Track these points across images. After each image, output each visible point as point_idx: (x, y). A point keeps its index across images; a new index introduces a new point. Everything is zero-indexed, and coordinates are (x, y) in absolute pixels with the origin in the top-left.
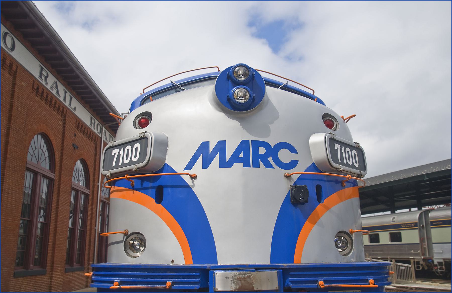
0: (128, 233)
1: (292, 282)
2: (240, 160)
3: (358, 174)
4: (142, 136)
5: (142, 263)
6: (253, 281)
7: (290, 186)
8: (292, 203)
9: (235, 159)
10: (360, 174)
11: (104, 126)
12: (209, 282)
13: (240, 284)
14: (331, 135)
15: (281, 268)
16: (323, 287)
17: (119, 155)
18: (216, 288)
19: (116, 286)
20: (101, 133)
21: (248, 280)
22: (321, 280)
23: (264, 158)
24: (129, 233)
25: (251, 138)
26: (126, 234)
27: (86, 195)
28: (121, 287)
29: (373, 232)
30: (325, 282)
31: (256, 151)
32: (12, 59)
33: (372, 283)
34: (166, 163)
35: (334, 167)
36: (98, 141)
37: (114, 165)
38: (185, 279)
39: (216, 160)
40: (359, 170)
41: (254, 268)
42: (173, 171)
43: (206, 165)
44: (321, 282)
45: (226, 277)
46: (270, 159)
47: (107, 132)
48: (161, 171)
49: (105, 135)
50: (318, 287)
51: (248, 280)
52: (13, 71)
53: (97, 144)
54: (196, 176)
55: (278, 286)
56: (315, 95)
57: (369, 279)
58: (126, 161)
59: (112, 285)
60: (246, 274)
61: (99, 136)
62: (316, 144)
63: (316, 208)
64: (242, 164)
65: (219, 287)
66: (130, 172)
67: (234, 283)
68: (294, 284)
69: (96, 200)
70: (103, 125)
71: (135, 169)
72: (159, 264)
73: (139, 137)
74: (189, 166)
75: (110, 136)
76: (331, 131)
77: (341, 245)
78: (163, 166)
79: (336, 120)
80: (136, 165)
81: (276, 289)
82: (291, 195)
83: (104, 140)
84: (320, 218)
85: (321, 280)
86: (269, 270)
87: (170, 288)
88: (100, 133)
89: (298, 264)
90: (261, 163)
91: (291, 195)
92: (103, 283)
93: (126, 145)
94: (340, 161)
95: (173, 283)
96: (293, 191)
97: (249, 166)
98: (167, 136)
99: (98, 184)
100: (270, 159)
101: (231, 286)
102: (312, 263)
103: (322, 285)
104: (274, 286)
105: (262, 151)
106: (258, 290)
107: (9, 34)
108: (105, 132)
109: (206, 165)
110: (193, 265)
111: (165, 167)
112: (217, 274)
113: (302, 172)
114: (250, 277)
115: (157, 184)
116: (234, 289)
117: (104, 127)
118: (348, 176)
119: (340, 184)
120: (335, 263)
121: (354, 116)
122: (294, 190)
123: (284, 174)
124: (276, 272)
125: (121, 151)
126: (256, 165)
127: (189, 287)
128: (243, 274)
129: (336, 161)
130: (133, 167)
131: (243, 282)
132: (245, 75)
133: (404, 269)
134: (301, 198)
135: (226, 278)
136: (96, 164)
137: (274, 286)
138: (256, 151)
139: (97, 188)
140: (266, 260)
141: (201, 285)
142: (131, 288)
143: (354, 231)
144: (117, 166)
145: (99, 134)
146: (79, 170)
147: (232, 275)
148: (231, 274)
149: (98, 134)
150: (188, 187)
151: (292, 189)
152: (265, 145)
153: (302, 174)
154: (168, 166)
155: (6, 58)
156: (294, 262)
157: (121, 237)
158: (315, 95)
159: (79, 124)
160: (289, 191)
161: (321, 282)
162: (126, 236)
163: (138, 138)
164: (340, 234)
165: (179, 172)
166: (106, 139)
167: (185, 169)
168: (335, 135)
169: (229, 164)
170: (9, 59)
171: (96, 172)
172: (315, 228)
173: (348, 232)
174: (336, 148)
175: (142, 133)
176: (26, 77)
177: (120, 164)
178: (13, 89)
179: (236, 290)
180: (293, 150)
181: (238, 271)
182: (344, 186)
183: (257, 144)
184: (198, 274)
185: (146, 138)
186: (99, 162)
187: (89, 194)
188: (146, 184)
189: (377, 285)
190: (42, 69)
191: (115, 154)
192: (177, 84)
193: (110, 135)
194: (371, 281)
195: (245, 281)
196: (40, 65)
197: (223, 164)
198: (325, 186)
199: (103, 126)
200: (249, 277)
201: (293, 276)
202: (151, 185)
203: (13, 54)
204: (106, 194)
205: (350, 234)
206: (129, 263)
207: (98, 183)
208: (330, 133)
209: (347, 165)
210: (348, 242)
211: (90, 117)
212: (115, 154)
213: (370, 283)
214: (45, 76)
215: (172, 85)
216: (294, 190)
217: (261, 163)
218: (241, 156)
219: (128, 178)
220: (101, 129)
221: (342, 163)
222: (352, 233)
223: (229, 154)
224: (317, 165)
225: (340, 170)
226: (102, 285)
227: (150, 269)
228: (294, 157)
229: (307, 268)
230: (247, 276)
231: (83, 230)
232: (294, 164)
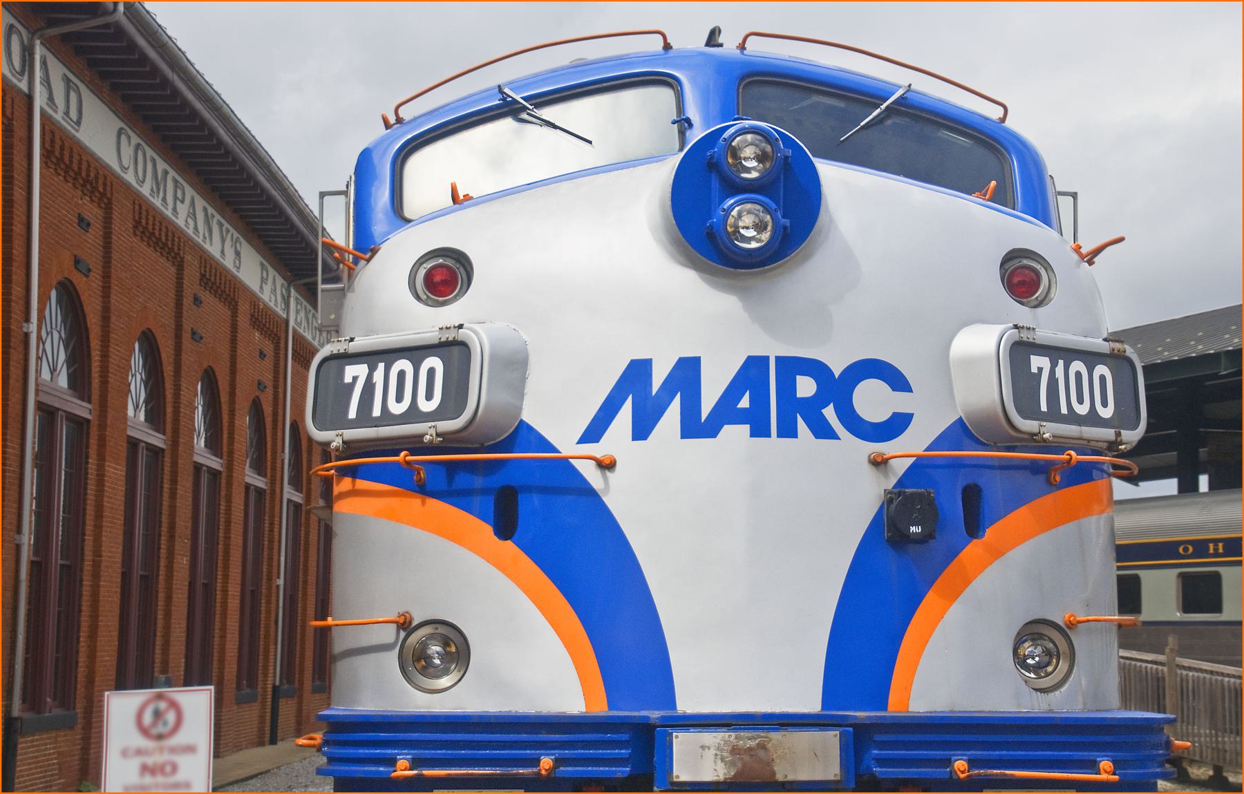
0: (410, 623)
1: (881, 762)
2: (739, 417)
3: (1107, 442)
4: (451, 339)
5: (461, 709)
6: (774, 757)
7: (885, 490)
8: (888, 541)
9: (726, 412)
10: (1116, 439)
11: (38, 34)
12: (655, 759)
13: (739, 765)
14: (1019, 332)
15: (849, 722)
16: (965, 778)
17: (369, 387)
18: (675, 773)
19: (402, 770)
20: (26, 73)
21: (761, 753)
22: (960, 757)
23: (811, 410)
24: (415, 623)
25: (773, 349)
26: (405, 625)
27: (79, 425)
28: (424, 772)
30: (972, 763)
31: (787, 387)
33: (1108, 770)
34: (524, 419)
35: (1023, 430)
36: (16, 113)
37: (352, 414)
38: (590, 750)
39: (673, 414)
40: (1112, 427)
41: (776, 723)
42: (547, 446)
43: (641, 430)
44: (960, 765)
45: (700, 745)
46: (829, 413)
47: (53, 63)
48: (507, 445)
49: (47, 81)
50: (951, 777)
51: (761, 753)
53: (12, 131)
54: (615, 462)
55: (841, 771)
56: (1008, 123)
57: (1100, 759)
58: (397, 409)
59: (391, 769)
60: (755, 739)
61: (20, 91)
62: (970, 362)
63: (960, 555)
64: (745, 429)
65: (682, 772)
66: (415, 445)
67: (722, 761)
68: (884, 767)
69: (19, 407)
70: (38, 30)
71: (431, 435)
72: (510, 711)
73: (440, 339)
74: (593, 433)
75: (68, 81)
76: (1022, 314)
77: (1037, 659)
78: (513, 428)
79: (1048, 267)
80: (433, 424)
81: (836, 779)
82: (887, 517)
83: (42, 110)
84: (970, 582)
85: (960, 757)
86: (817, 729)
87: (549, 774)
88: (22, 73)
89: (901, 712)
90: (801, 424)
91: (885, 517)
92: (362, 765)
93: (394, 355)
94: (1044, 408)
96: (893, 506)
97: (767, 434)
98: (525, 337)
99: (25, 330)
100: (829, 413)
101: (715, 770)
102: (942, 712)
103: (963, 772)
104: (832, 771)
105: (806, 387)
106: (786, 780)
108: (44, 63)
109: (641, 430)
110: (610, 712)
111: (523, 435)
112: (677, 737)
113: (920, 450)
114: (765, 745)
115: (498, 480)
116: (722, 778)
117: (38, 42)
118: (1068, 455)
119: (1042, 478)
120: (1010, 712)
121: (1121, 240)
122: (895, 503)
123: (869, 456)
124: (834, 733)
125: (375, 373)
126: (788, 431)
127: (603, 771)
128: (748, 740)
129: (1030, 410)
130: (428, 431)
131: (747, 758)
132: (762, 158)
133: (676, 713)
134: (913, 529)
135: (703, 747)
136: (12, 230)
137: (832, 771)
138: (787, 387)
139: (21, 349)
140: (810, 702)
141: (632, 767)
142: (450, 774)
143: (1078, 619)
144: (364, 417)
145: (20, 81)
146: (54, 326)
147: (718, 741)
148: (713, 738)
149: (15, 81)
150: (591, 493)
151: (890, 501)
152: (815, 368)
153: (919, 458)
154: (530, 428)
156: (890, 708)
157: (388, 634)
158: (1008, 123)
159: (64, 149)
160: (879, 506)
161: (960, 765)
162: (404, 629)
163: (436, 341)
164: (1034, 630)
165: (565, 452)
166: (51, 98)
167: (581, 441)
168: (1034, 329)
169: (709, 429)
171: (14, 269)
172: (956, 612)
173: (1060, 624)
174: (1034, 370)
175: (450, 328)
177: (377, 412)
178: (107, 225)
179: (729, 778)
180: (898, 382)
181: (734, 729)
182: (1055, 483)
183: (791, 367)
184: (625, 737)
185: (463, 345)
186: (24, 218)
187: (88, 421)
188: (462, 480)
189: (1118, 777)
191: (355, 379)
192: (518, 98)
193: (220, 222)
194: (1105, 764)
195: (752, 756)
197: (693, 427)
198: (994, 487)
199: (33, 34)
200: (762, 746)
201: (883, 745)
202: (479, 482)
204: (55, 370)
205: (1065, 629)
206: (418, 708)
207: (25, 325)
208: (1016, 327)
209: (1073, 418)
210: (1061, 652)
211: (63, 80)
212: (355, 379)
213: (1102, 771)
215: (504, 99)
216: (895, 503)
217: (801, 424)
218: (745, 403)
219: (408, 463)
220: (27, 52)
221: (1054, 415)
222: (1072, 625)
223: (710, 397)
224: (970, 424)
225: (1043, 438)
226: (362, 769)
227: (510, 724)
229: (925, 725)
230: (757, 742)
231: (67, 566)
232: (897, 425)
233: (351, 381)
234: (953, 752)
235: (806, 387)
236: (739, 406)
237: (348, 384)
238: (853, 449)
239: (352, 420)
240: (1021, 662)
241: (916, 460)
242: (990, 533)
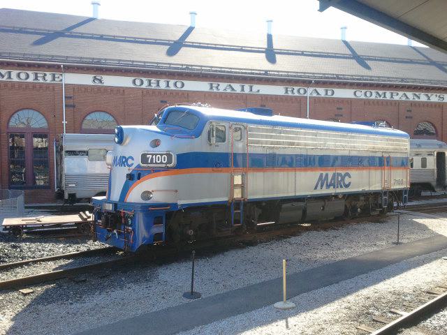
180: (133, 159)
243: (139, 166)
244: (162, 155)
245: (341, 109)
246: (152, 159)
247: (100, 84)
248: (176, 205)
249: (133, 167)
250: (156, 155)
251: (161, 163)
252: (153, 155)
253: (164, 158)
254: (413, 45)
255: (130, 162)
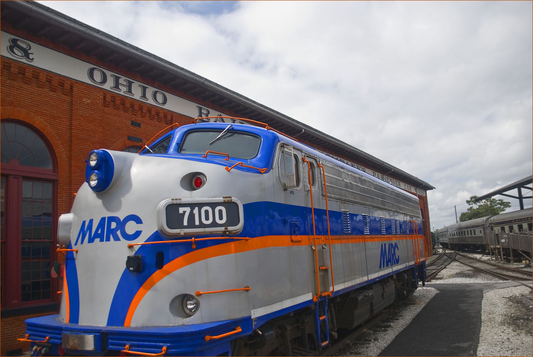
9: (96, 235)
29: (520, 223)
32: (166, 111)
52: (169, 120)
95: (50, 338)
97: (103, 241)
100: (119, 233)
107: (159, 91)
138: (109, 225)
155: (159, 112)
170: (162, 113)
176: (184, 121)
180: (138, 220)
183: (112, 219)
190: (200, 109)
191: (184, 212)
196: (198, 106)
201: (112, 339)
203: (166, 107)
214: (206, 113)
228: (138, 227)
232: (138, 234)
233: (182, 212)
234: (127, 342)
235: (114, 225)
236: (119, 231)
237: (181, 214)
238: (125, 243)
239: (99, 233)
240: (197, 306)
241: (141, 246)
242: (165, 267)
243: (157, 236)
244: (213, 205)
245: (133, 123)
246: (192, 216)
247: (24, 60)
248: (246, 321)
249: (140, 241)
250: (200, 205)
251: (214, 224)
252: (192, 206)
253: (220, 212)
254: (442, 280)
255: (131, 228)
